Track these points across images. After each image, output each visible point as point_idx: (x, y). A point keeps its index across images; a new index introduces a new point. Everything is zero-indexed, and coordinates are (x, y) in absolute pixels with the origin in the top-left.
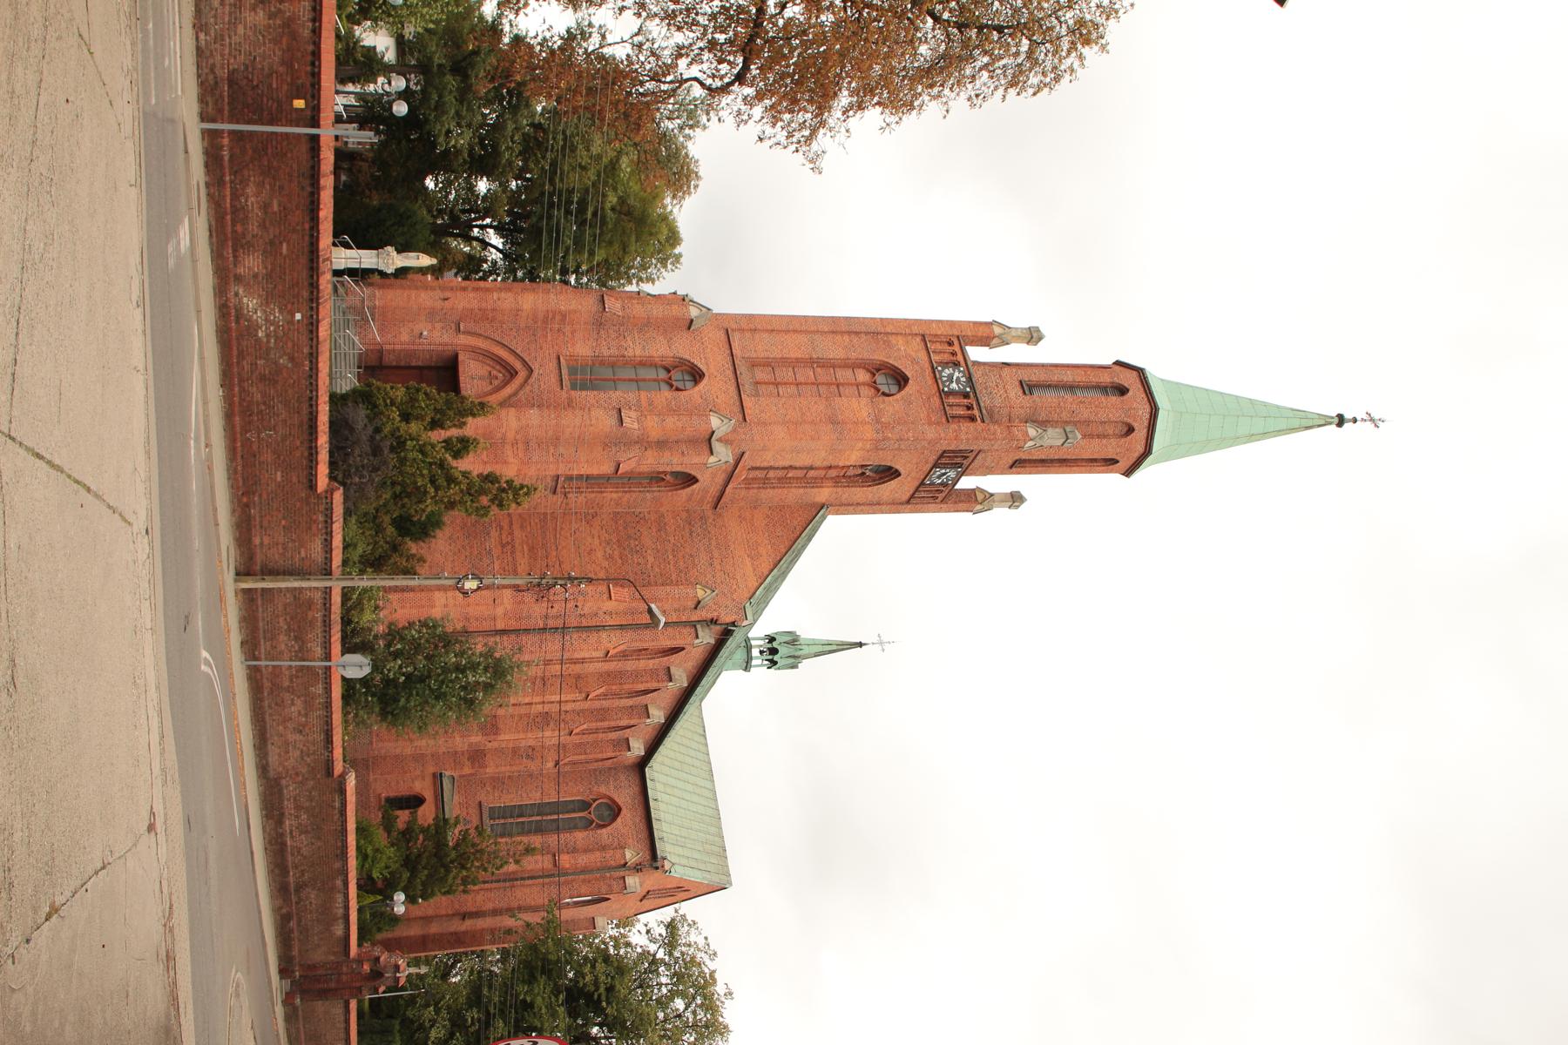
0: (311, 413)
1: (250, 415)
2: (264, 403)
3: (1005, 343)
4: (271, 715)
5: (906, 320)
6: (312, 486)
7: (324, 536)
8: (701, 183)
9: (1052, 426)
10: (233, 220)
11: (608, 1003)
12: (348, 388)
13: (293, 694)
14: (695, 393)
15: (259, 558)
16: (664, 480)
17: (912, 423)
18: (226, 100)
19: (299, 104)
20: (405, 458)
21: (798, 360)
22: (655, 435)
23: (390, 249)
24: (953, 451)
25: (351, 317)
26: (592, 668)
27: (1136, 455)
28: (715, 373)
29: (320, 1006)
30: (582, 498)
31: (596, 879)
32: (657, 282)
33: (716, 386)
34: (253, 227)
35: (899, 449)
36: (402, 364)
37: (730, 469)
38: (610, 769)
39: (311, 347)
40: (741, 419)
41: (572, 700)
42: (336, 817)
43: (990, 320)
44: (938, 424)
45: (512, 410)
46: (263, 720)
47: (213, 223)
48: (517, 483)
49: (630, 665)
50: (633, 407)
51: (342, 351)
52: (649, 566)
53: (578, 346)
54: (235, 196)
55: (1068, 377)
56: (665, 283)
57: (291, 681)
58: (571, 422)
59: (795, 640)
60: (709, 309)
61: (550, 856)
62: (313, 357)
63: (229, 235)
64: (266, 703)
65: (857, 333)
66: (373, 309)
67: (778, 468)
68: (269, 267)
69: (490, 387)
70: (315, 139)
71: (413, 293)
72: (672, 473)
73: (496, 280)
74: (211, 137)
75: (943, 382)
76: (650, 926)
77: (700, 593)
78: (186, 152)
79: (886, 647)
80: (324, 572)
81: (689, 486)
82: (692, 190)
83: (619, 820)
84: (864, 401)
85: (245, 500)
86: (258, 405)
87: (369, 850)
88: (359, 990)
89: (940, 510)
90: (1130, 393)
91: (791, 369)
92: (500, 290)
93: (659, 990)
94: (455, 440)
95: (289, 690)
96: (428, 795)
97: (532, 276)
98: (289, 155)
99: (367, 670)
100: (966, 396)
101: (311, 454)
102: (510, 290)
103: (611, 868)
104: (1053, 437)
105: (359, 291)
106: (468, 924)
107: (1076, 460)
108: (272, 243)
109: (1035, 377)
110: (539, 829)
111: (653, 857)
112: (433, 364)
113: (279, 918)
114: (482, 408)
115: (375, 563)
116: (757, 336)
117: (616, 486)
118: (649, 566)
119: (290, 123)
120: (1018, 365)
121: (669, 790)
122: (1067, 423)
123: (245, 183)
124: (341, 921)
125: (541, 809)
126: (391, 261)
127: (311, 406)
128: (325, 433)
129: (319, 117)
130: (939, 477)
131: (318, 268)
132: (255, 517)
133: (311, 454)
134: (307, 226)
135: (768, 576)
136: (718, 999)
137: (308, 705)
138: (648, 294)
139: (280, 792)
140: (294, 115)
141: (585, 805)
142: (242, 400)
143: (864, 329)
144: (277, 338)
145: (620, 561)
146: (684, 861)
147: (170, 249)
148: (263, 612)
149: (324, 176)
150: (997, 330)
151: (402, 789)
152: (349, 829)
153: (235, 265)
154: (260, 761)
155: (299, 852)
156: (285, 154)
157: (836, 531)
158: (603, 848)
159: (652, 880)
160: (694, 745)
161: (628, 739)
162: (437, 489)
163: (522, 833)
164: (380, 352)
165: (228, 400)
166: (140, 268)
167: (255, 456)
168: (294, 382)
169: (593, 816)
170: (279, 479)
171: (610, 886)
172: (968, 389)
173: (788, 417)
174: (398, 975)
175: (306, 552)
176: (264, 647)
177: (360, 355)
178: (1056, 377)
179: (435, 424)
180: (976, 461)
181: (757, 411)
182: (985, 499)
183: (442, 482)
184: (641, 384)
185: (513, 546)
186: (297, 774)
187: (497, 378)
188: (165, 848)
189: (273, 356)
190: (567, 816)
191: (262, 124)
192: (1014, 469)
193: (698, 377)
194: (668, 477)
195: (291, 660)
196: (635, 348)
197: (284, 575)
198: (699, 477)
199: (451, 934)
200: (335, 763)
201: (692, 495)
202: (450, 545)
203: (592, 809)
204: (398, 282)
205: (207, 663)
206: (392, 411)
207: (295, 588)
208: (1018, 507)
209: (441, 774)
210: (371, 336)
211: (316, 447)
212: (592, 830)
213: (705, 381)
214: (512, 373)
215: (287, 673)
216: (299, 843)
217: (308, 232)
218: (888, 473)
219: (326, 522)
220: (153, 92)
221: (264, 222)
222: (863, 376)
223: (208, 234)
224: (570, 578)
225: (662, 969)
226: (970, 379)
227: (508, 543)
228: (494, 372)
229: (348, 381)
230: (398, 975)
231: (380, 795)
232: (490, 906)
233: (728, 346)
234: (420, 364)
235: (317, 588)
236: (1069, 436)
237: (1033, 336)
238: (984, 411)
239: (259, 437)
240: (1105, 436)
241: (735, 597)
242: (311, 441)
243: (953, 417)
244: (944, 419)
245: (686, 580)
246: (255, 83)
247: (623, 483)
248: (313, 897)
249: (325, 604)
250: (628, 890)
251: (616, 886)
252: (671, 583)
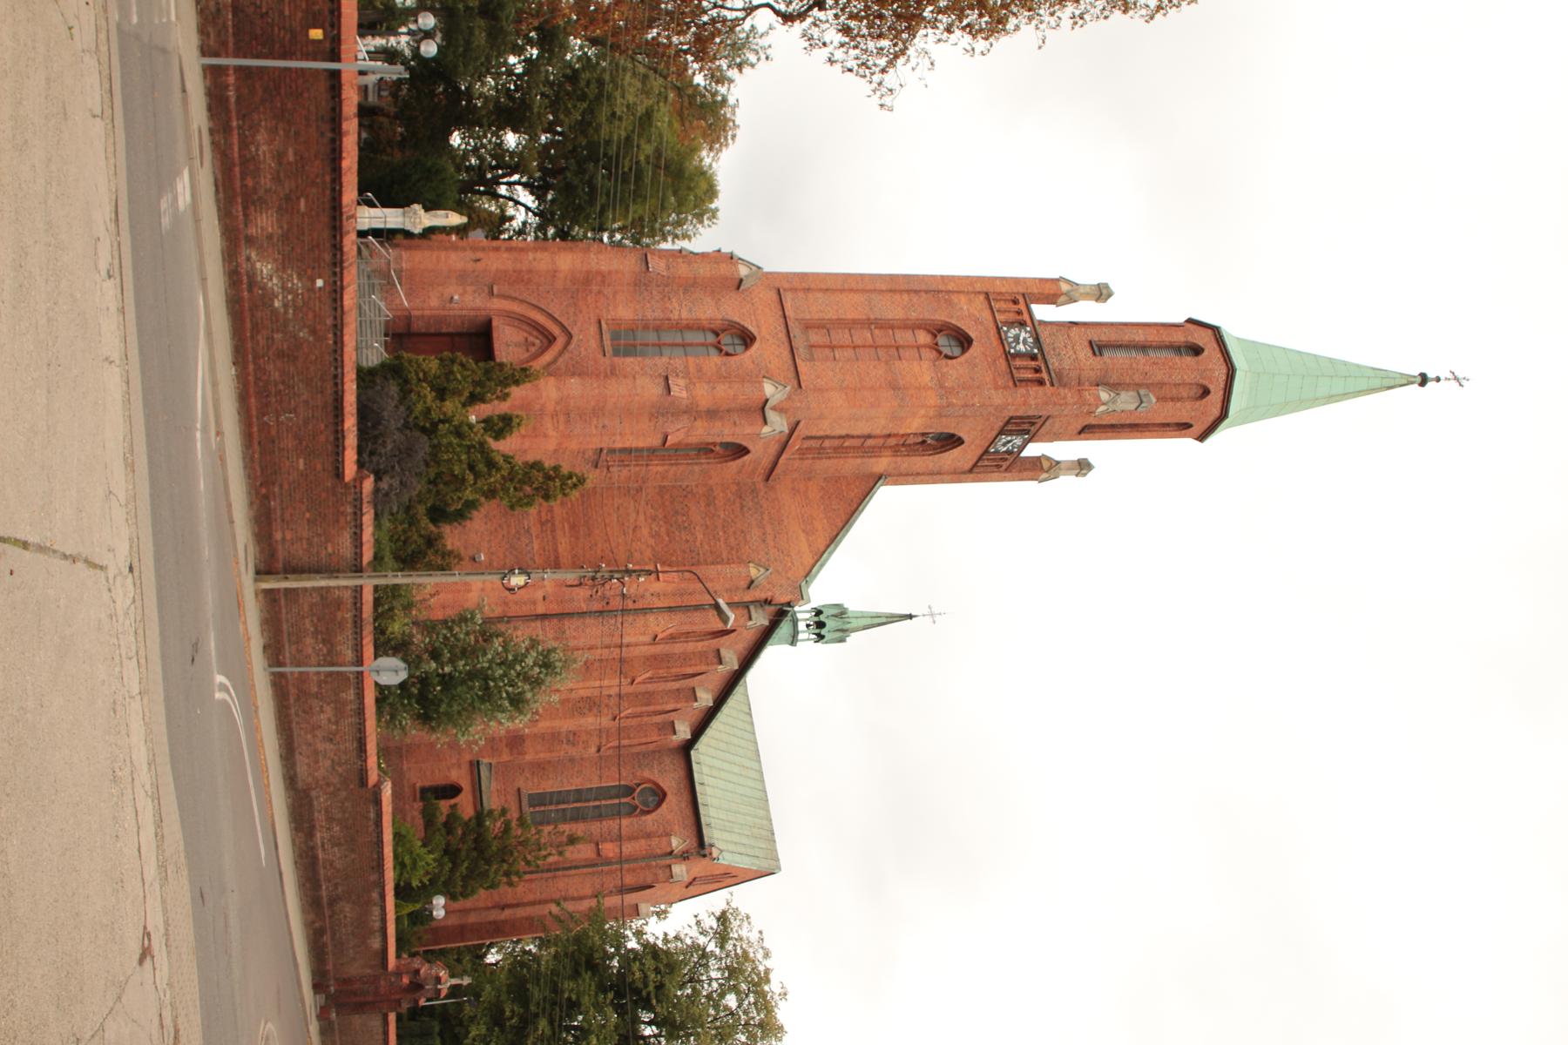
0: (336, 392)
1: (267, 396)
2: (283, 383)
3: (1072, 300)
4: (298, 723)
5: (968, 277)
6: (338, 473)
7: (353, 530)
8: (738, 132)
9: (1123, 389)
10: (242, 173)
11: (658, 1001)
12: (376, 362)
13: (321, 700)
14: (747, 358)
15: (281, 554)
16: (712, 451)
17: (978, 387)
18: (231, 30)
19: (316, 34)
20: (439, 444)
21: (854, 321)
22: (704, 403)
23: (417, 207)
24: (1021, 418)
25: (376, 282)
26: (637, 651)
27: (1211, 419)
28: (768, 337)
29: (357, 1020)
30: (625, 472)
31: (642, 868)
32: (693, 239)
33: (769, 349)
34: (266, 181)
35: (964, 416)
36: (432, 331)
37: (784, 439)
38: (654, 752)
39: (335, 318)
40: (796, 386)
41: (611, 684)
42: (371, 829)
43: (1057, 277)
44: (1005, 388)
45: (552, 380)
46: (290, 729)
47: (220, 177)
48: (565, 470)
49: (678, 648)
50: (681, 375)
51: (368, 319)
52: (698, 544)
53: (621, 308)
54: (244, 145)
55: (1140, 337)
56: (703, 239)
57: (320, 687)
58: (617, 390)
59: (842, 613)
60: (759, 268)
61: (593, 845)
62: (338, 329)
63: (238, 190)
64: (293, 711)
65: (916, 292)
66: (399, 273)
67: (833, 437)
68: (285, 227)
69: (526, 355)
70: (335, 75)
71: (443, 254)
72: (721, 443)
73: (526, 240)
74: (214, 75)
75: (1009, 344)
76: (699, 918)
77: (753, 572)
78: (184, 91)
79: (937, 618)
80: (354, 568)
81: (739, 457)
82: (730, 141)
83: (664, 805)
84: (926, 364)
85: (264, 491)
86: (276, 385)
87: (407, 859)
88: (399, 1002)
89: (1004, 479)
90: (1206, 353)
91: (847, 331)
92: (535, 249)
93: (710, 985)
94: (496, 418)
95: (317, 696)
96: (465, 784)
97: (563, 235)
98: (306, 95)
99: (403, 676)
100: (1033, 358)
101: (337, 439)
102: (545, 249)
103: (655, 857)
104: (1126, 402)
105: (385, 254)
106: (507, 913)
107: (1147, 425)
108: (288, 198)
109: (1105, 336)
110: (578, 816)
111: (701, 846)
112: (465, 330)
113: (311, 932)
114: (521, 375)
115: (408, 561)
116: (810, 295)
117: (663, 458)
118: (698, 544)
119: (306, 57)
120: (1085, 324)
121: (715, 773)
122: (1139, 385)
123: (254, 128)
124: (377, 934)
125: (579, 795)
126: (418, 220)
127: (336, 384)
128: (352, 415)
129: (339, 49)
130: (1004, 445)
131: (341, 227)
132: (275, 509)
133: (337, 439)
134: (328, 178)
135: (824, 552)
136: (772, 997)
137: (339, 712)
138: (691, 253)
139: (311, 805)
140: (310, 48)
141: (629, 791)
142: (257, 379)
143: (923, 287)
144: (296, 309)
145: (667, 539)
146: (732, 847)
147: (164, 205)
148: (287, 613)
149: (347, 120)
150: (1064, 287)
151: (437, 778)
152: (385, 840)
153: (246, 226)
154: (288, 771)
155: (331, 865)
156: (301, 94)
157: (888, 500)
158: (649, 836)
159: (699, 867)
160: (740, 724)
161: (673, 722)
162: (477, 475)
163: (565, 821)
164: (408, 319)
165: (242, 379)
166: (112, 227)
167: (273, 442)
168: (316, 359)
169: (636, 802)
170: (301, 466)
171: (656, 874)
172: (1036, 351)
173: (846, 382)
174: (439, 987)
175: (333, 547)
176: (288, 651)
177: (387, 323)
178: (1127, 337)
179: (474, 399)
180: (1044, 427)
181: (813, 377)
182: (1051, 468)
183: (481, 467)
184: (688, 349)
185: (553, 525)
186: (328, 785)
187: (534, 345)
188: (166, 969)
189: (291, 329)
190: (609, 802)
191: (274, 58)
192: (1082, 435)
193: (748, 341)
194: (718, 448)
195: (319, 665)
196: (681, 310)
197: (310, 572)
198: (750, 447)
199: (490, 923)
200: (369, 773)
201: (743, 466)
202: (486, 523)
203: (636, 794)
204: (424, 243)
205: (223, 688)
206: (422, 387)
207: (322, 588)
208: (1085, 475)
209: (478, 762)
210: (398, 301)
211: (343, 430)
212: (637, 816)
213: (756, 345)
214: (550, 339)
215: (315, 678)
216: (331, 856)
217: (328, 185)
218: (950, 441)
219: (355, 513)
220: (134, 9)
221: (278, 172)
222: (923, 338)
223: (213, 189)
224: (628, 572)
225: (712, 962)
226: (1037, 340)
227: (547, 521)
228: (531, 339)
229: (375, 354)
230: (439, 987)
231: (415, 784)
232: (531, 897)
233: (780, 307)
234: (451, 330)
235: (347, 587)
236: (1144, 399)
237: (1101, 293)
238: (1053, 375)
239: (278, 421)
240: (1179, 399)
241: (789, 575)
242: (337, 424)
243: (1020, 381)
244: (1011, 384)
245: (738, 558)
246: (264, 10)
247: (669, 456)
248: (347, 910)
249: (355, 604)
250: (675, 879)
251: (662, 875)
252: (721, 562)
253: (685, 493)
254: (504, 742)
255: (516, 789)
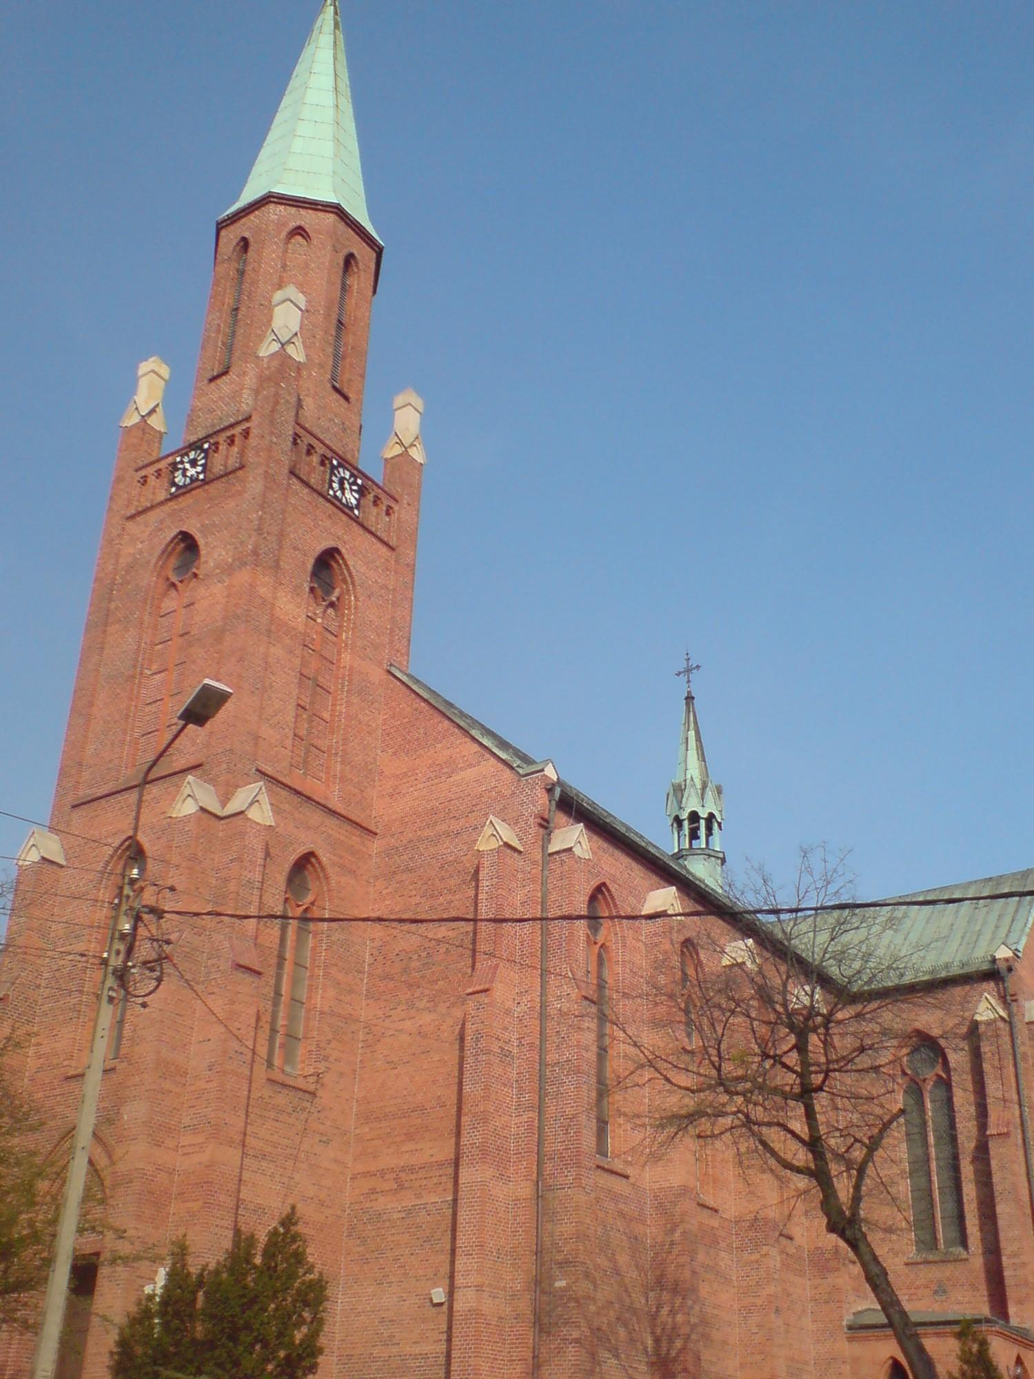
90: (247, 235)
135: (481, 744)
185: (403, 1169)
198: (302, 850)
201: (342, 866)
233: (95, 804)
241: (508, 793)
253: (380, 958)
254: (819, 1281)
255: (906, 1270)
